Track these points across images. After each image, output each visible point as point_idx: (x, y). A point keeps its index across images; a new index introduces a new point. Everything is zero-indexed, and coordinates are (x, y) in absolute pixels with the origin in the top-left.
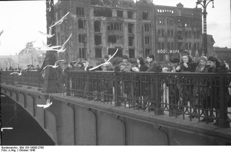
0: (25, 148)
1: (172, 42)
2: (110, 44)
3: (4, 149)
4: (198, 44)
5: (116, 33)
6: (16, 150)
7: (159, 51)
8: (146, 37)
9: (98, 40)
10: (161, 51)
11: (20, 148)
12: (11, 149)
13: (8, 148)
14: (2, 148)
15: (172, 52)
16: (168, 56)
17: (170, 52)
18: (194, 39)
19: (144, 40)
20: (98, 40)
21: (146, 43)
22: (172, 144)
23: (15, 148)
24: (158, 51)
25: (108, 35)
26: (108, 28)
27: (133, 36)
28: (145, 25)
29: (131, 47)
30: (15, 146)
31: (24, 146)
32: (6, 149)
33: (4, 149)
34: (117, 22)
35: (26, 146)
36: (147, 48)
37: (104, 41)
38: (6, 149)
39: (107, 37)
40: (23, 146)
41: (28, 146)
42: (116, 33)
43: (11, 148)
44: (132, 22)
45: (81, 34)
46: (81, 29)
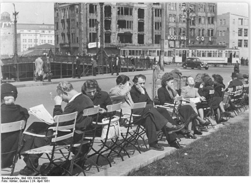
0: (27, 178)
1: (203, 29)
2: (119, 29)
3: (4, 180)
4: (202, 30)
5: (126, 18)
6: (18, 180)
7: (169, 37)
8: (156, 23)
9: (141, 26)
10: (172, 37)
11: (22, 178)
12: (9, 180)
13: (9, 178)
14: (2, 178)
15: (183, 39)
16: (178, 42)
17: (181, 39)
18: (208, 25)
19: (154, 25)
20: (141, 26)
21: (156, 28)
22: (217, 174)
23: (17, 179)
24: (168, 37)
25: (117, 20)
26: (119, 13)
27: (143, 21)
28: (156, 10)
29: (141, 33)
30: (16, 177)
31: (27, 177)
32: (6, 180)
33: (4, 180)
34: (128, 7)
35: (28, 177)
36: (157, 33)
37: (114, 25)
38: (6, 180)
39: (117, 21)
40: (25, 177)
41: (30, 177)
42: (126, 18)
43: (12, 179)
44: (142, 7)
45: (92, 19)
46: (92, 14)
